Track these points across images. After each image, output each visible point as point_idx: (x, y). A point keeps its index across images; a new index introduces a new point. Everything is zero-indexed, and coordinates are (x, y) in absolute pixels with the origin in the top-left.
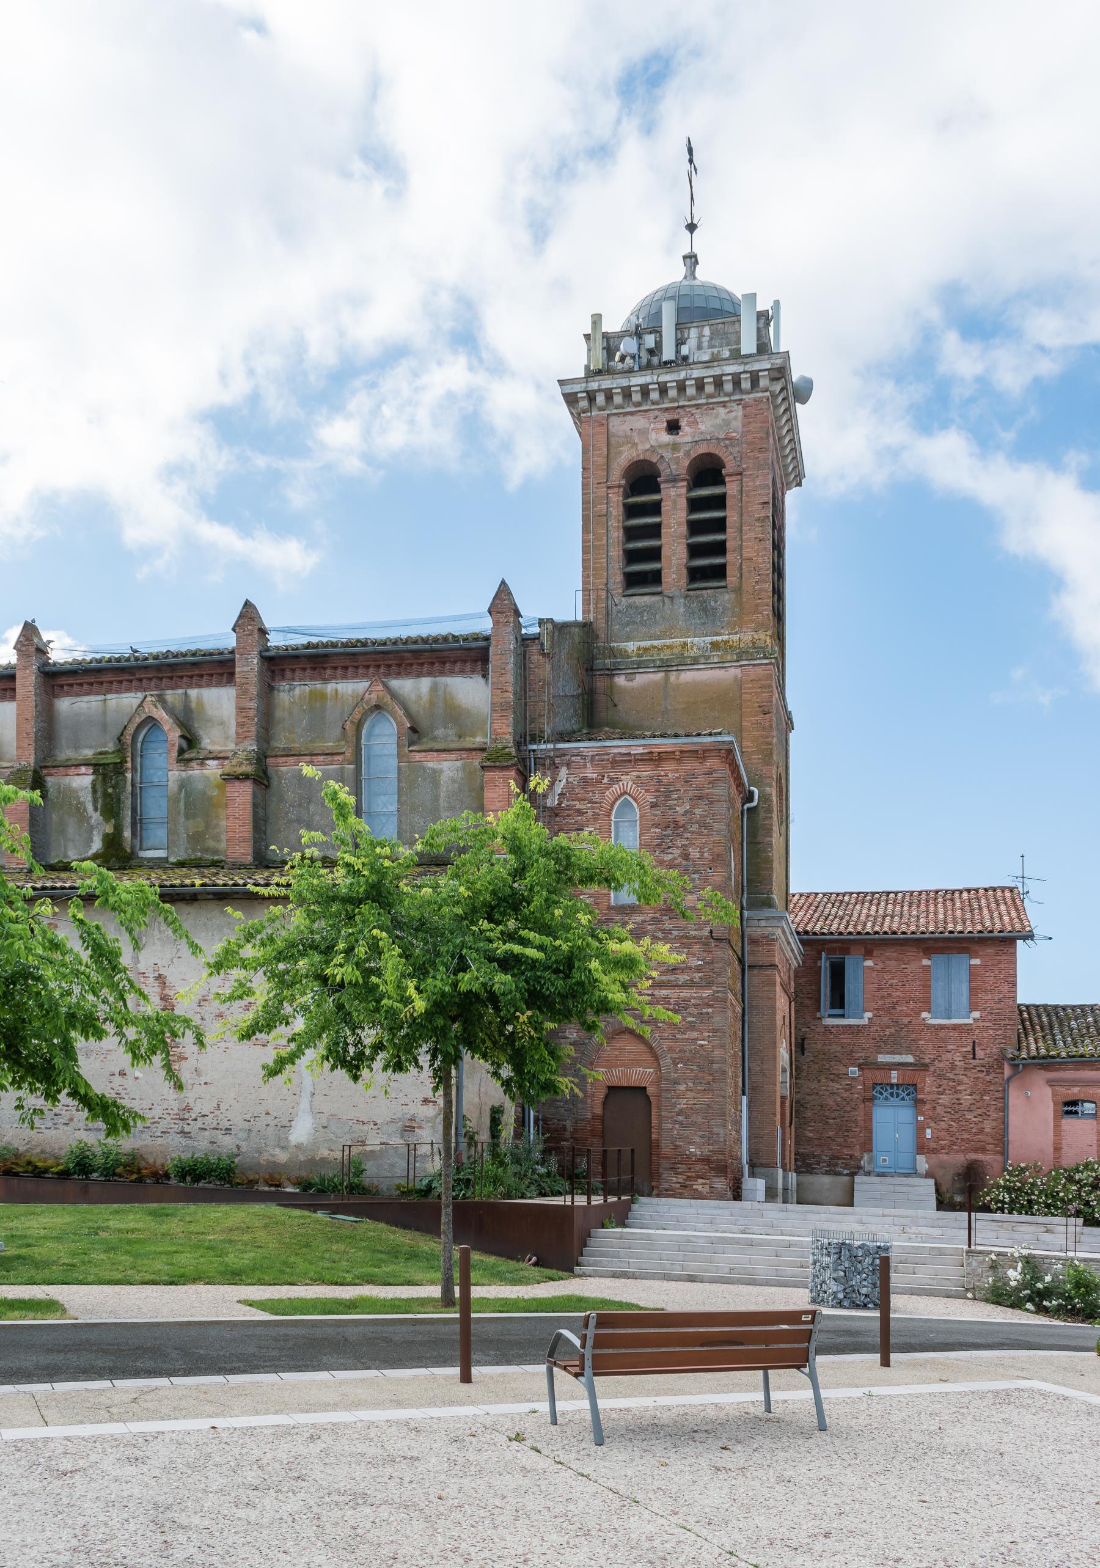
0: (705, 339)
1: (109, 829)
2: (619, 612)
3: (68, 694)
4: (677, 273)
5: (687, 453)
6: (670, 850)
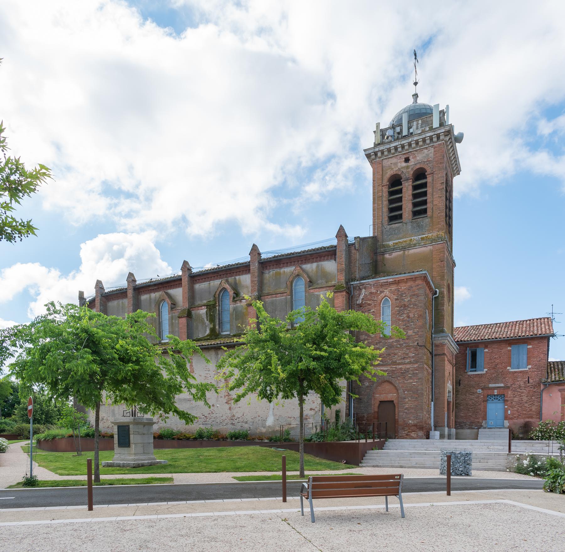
1: (212, 326)
3: (198, 283)
4: (410, 102)
5: (412, 169)
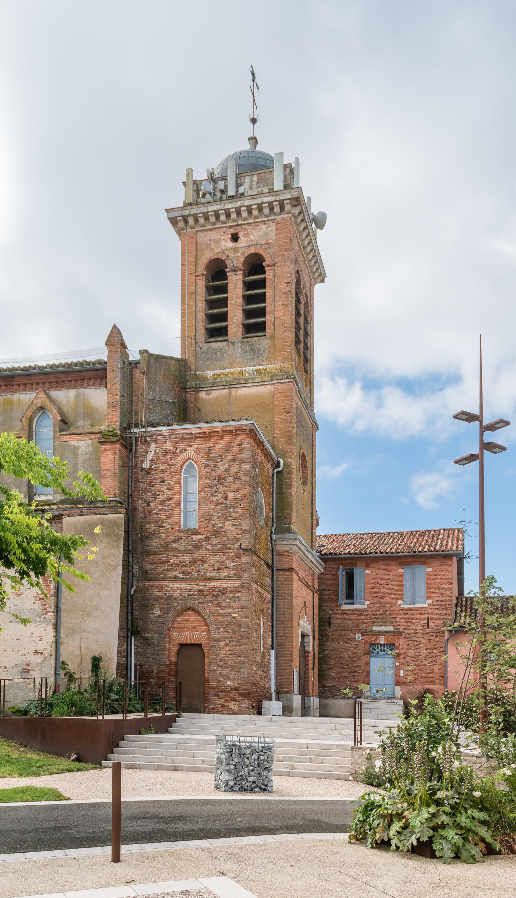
0: (254, 183)
2: (202, 353)
5: (243, 253)
6: (216, 494)
